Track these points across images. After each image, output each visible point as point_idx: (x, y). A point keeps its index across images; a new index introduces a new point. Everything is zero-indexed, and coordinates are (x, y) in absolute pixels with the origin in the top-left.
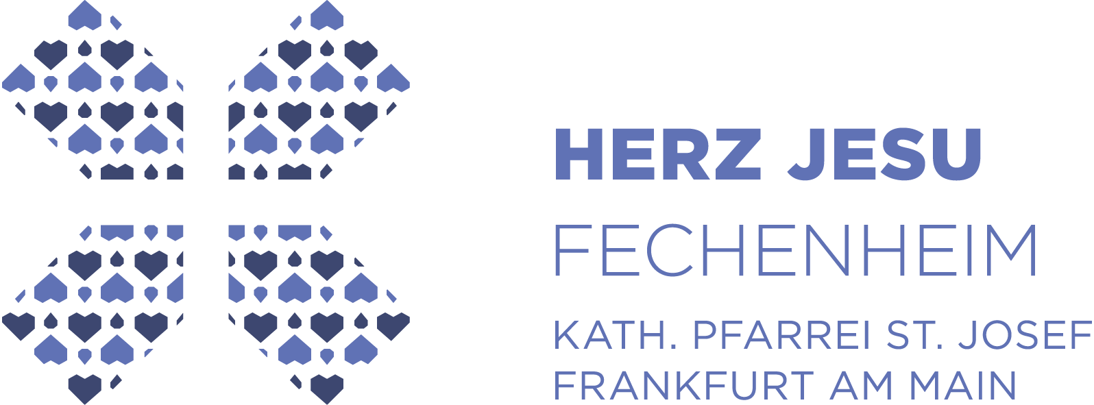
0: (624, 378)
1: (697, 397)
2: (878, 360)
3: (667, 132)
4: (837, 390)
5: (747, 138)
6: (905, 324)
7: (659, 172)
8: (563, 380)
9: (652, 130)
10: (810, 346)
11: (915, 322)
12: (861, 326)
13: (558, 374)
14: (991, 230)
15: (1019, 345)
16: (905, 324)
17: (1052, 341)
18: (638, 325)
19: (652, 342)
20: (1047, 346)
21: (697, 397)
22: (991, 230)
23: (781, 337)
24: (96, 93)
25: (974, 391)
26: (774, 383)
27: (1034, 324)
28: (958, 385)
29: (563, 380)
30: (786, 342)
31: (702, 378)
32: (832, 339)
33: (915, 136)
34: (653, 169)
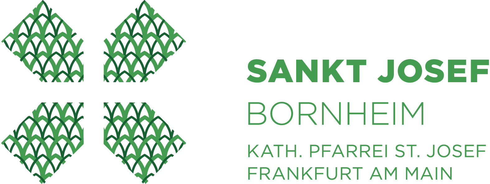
0: (376, 170)
1: (311, 179)
2: (391, 162)
3: (473, 61)
4: (373, 175)
5: (357, 64)
6: (403, 146)
7: (469, 78)
8: (252, 171)
9: (465, 60)
10: (361, 156)
11: (408, 145)
12: (384, 147)
13: (249, 168)
14: (404, 105)
15: (454, 155)
16: (403, 146)
17: (468, 154)
18: (285, 146)
19: (291, 154)
20: (466, 156)
21: (311, 179)
22: (404, 105)
23: (348, 152)
24: (45, 44)
25: (434, 176)
26: (344, 172)
27: (460, 146)
28: (427, 173)
29: (252, 171)
30: (350, 154)
31: (313, 171)
32: (371, 153)
33: (440, 63)
34: (465, 77)
